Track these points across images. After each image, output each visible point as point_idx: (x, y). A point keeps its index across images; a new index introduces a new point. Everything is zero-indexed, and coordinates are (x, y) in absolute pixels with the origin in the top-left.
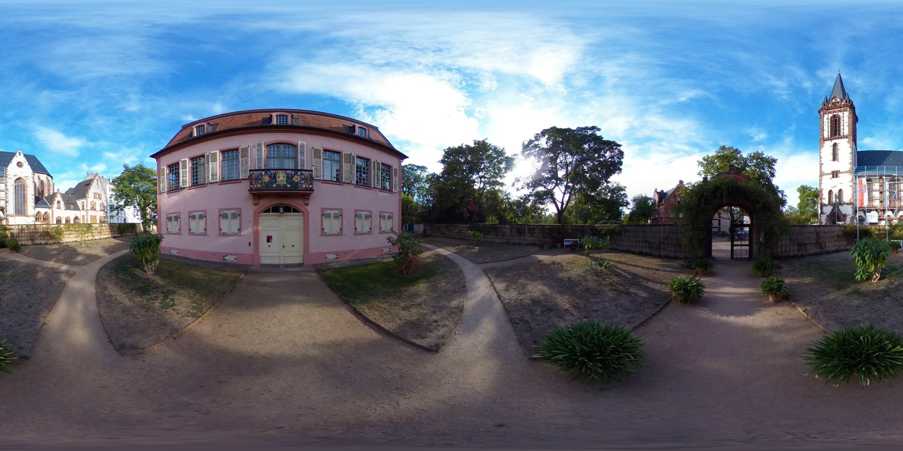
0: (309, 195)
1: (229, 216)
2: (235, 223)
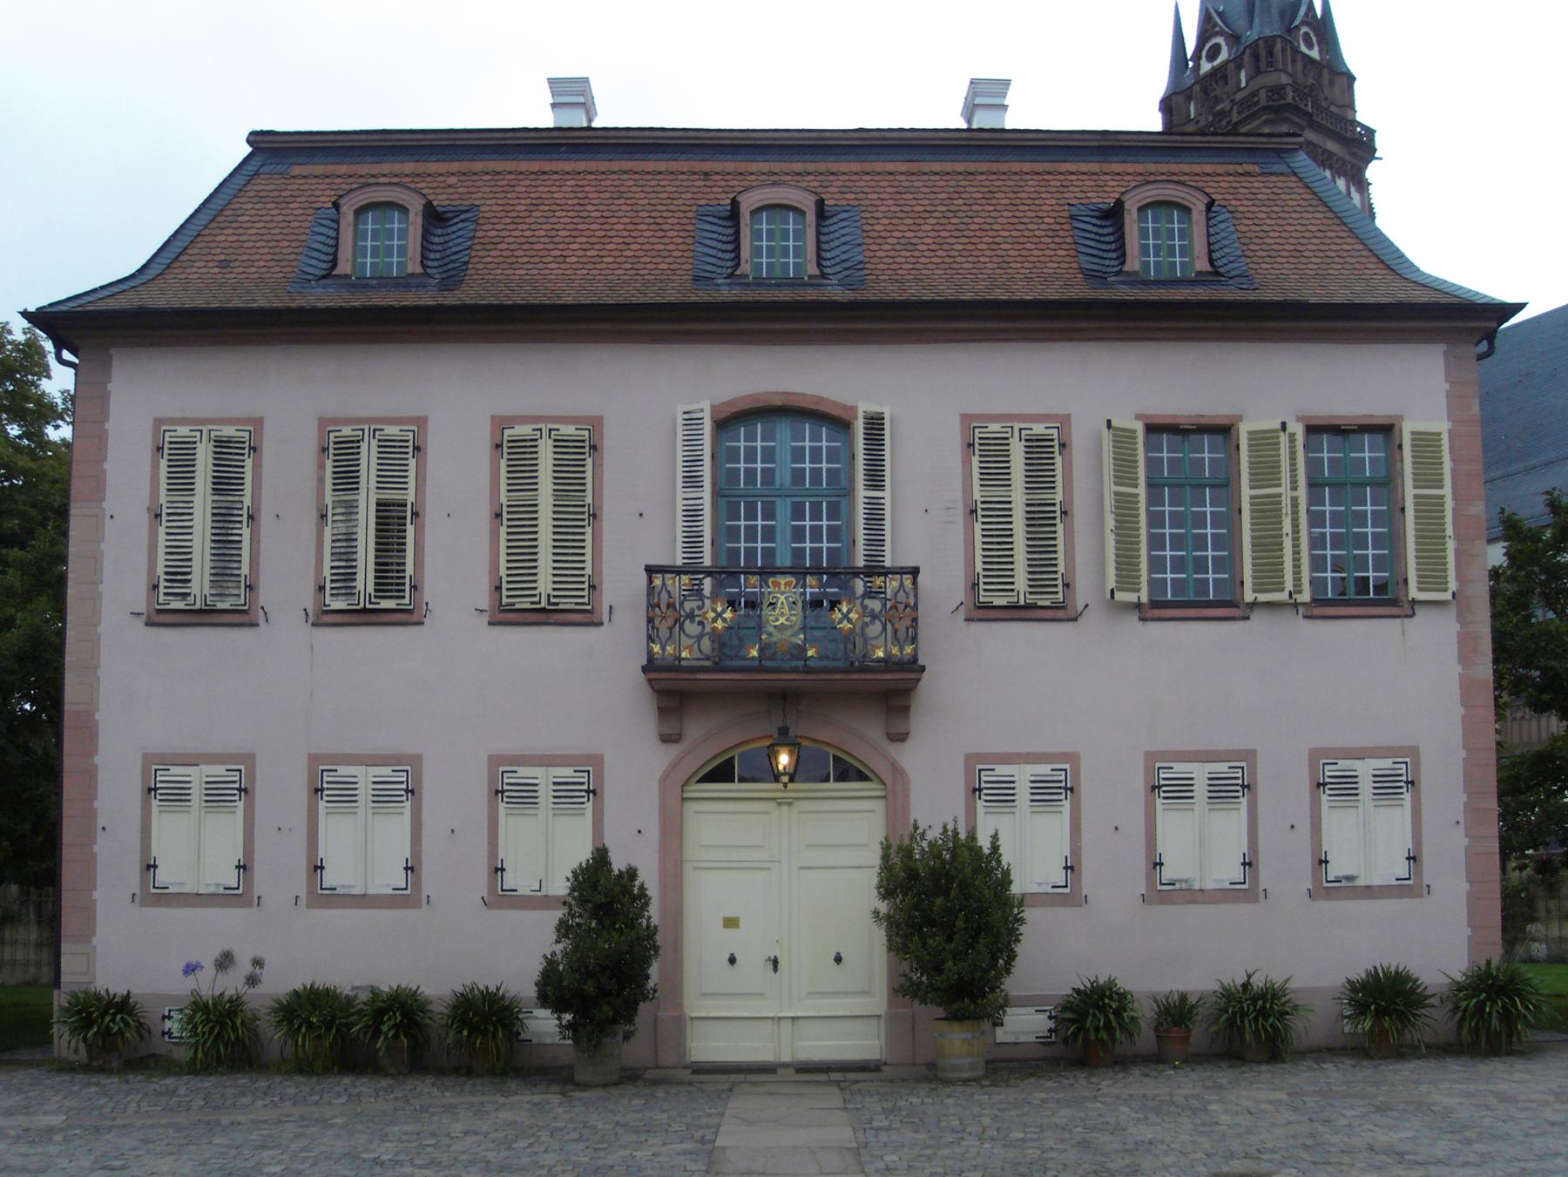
1: (545, 794)
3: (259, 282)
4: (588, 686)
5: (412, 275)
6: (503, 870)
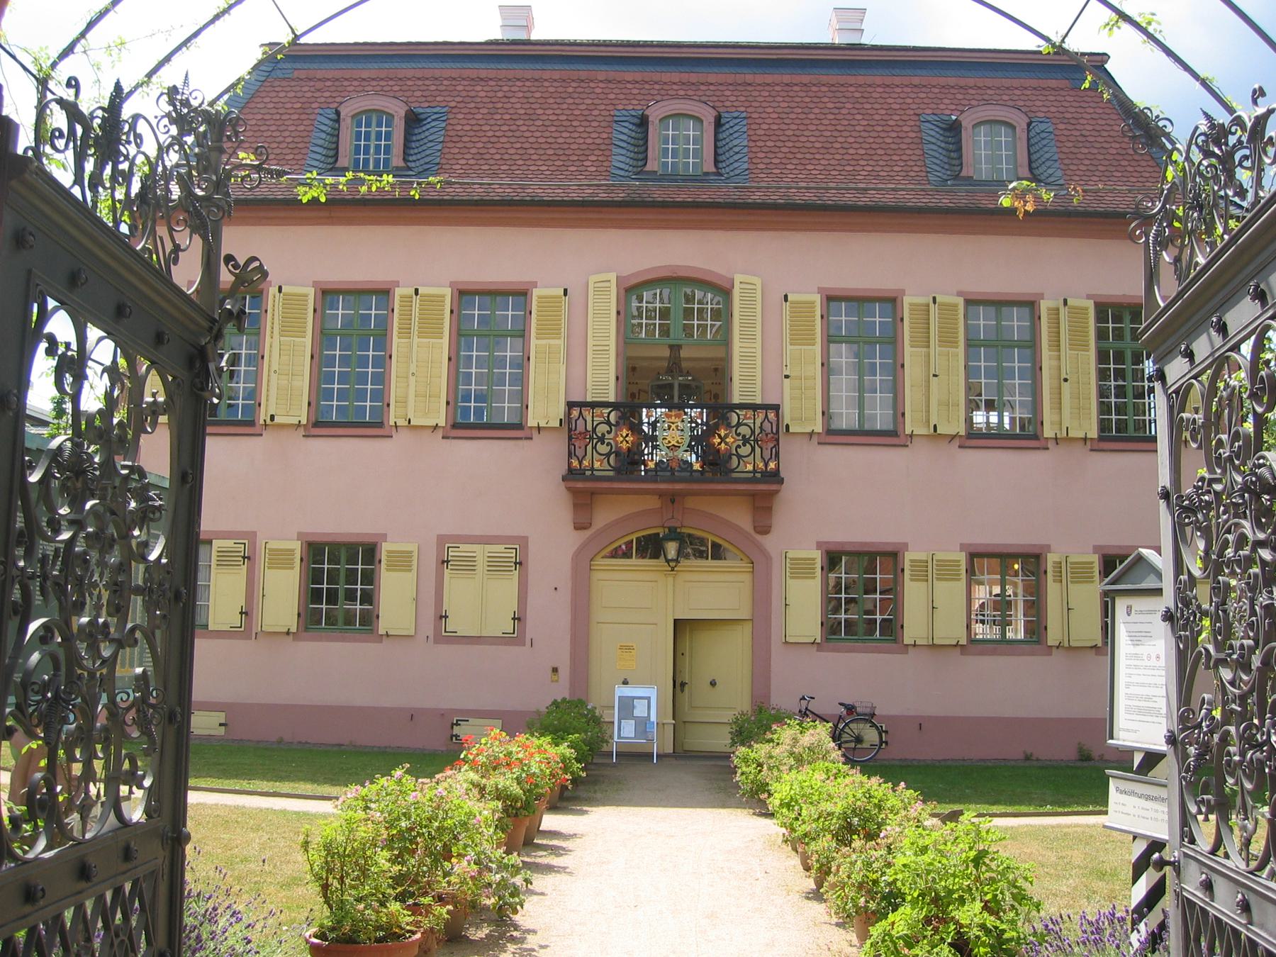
1: (481, 564)
4: (517, 486)
5: (707, 174)
6: (446, 617)
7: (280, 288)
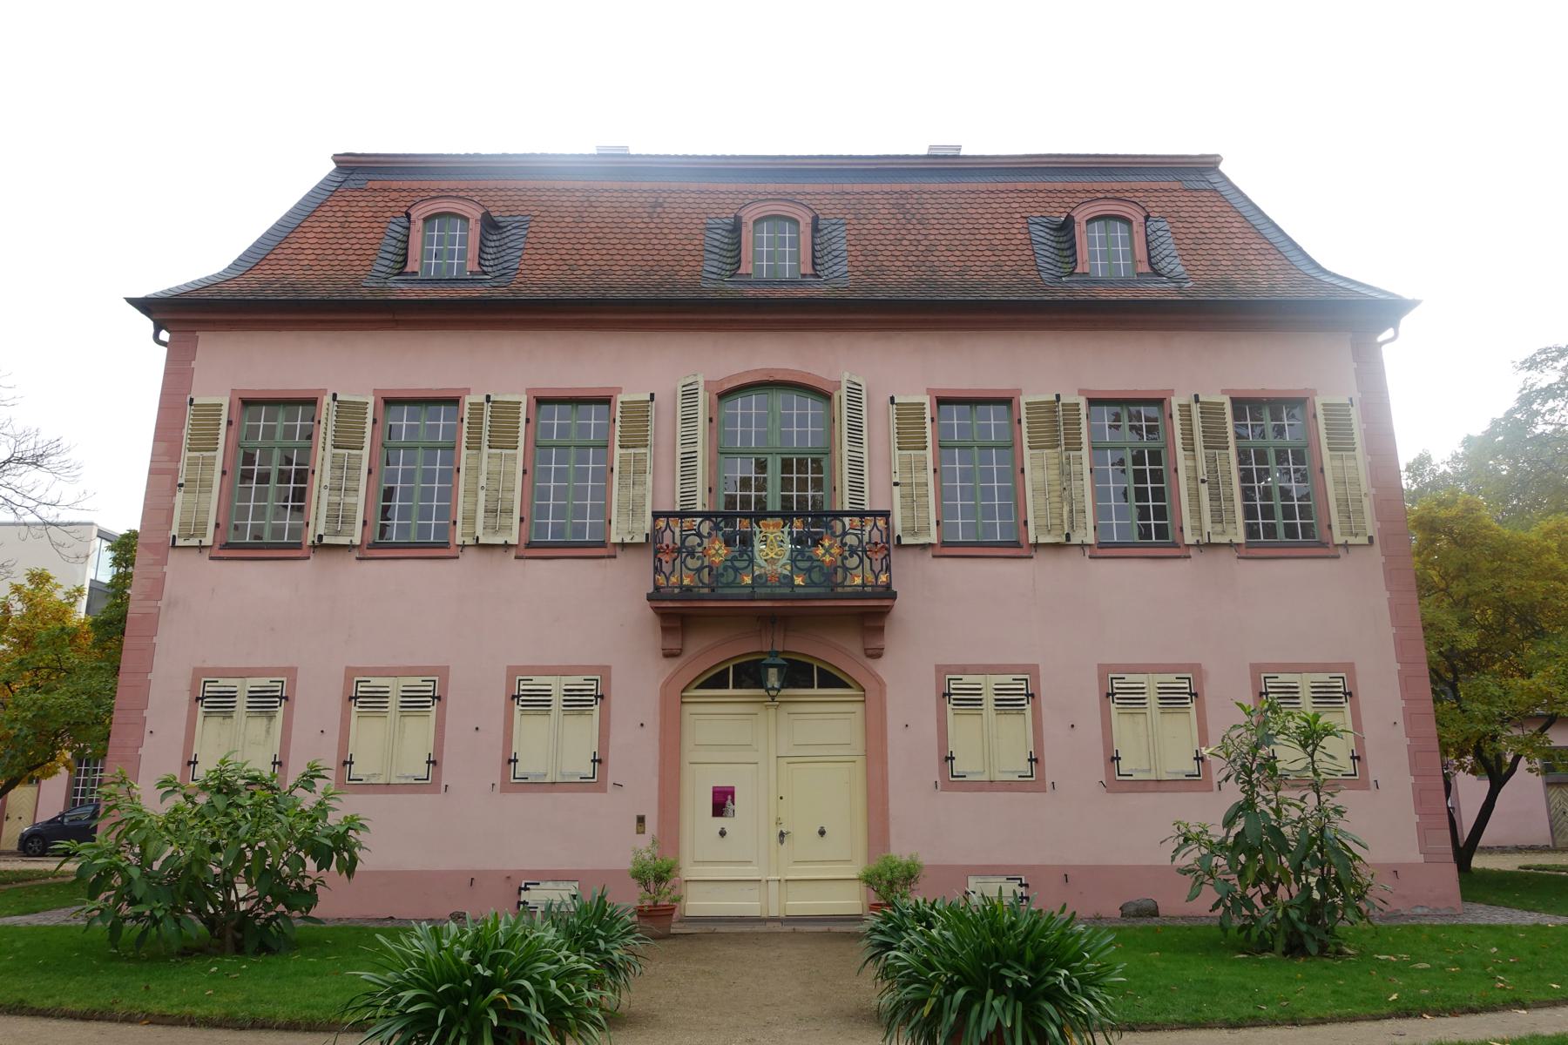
0: (883, 613)
1: (1152, 698)
2: (580, 735)
3: (308, 274)
4: (596, 613)
5: (804, 275)
6: (516, 761)
7: (335, 396)
